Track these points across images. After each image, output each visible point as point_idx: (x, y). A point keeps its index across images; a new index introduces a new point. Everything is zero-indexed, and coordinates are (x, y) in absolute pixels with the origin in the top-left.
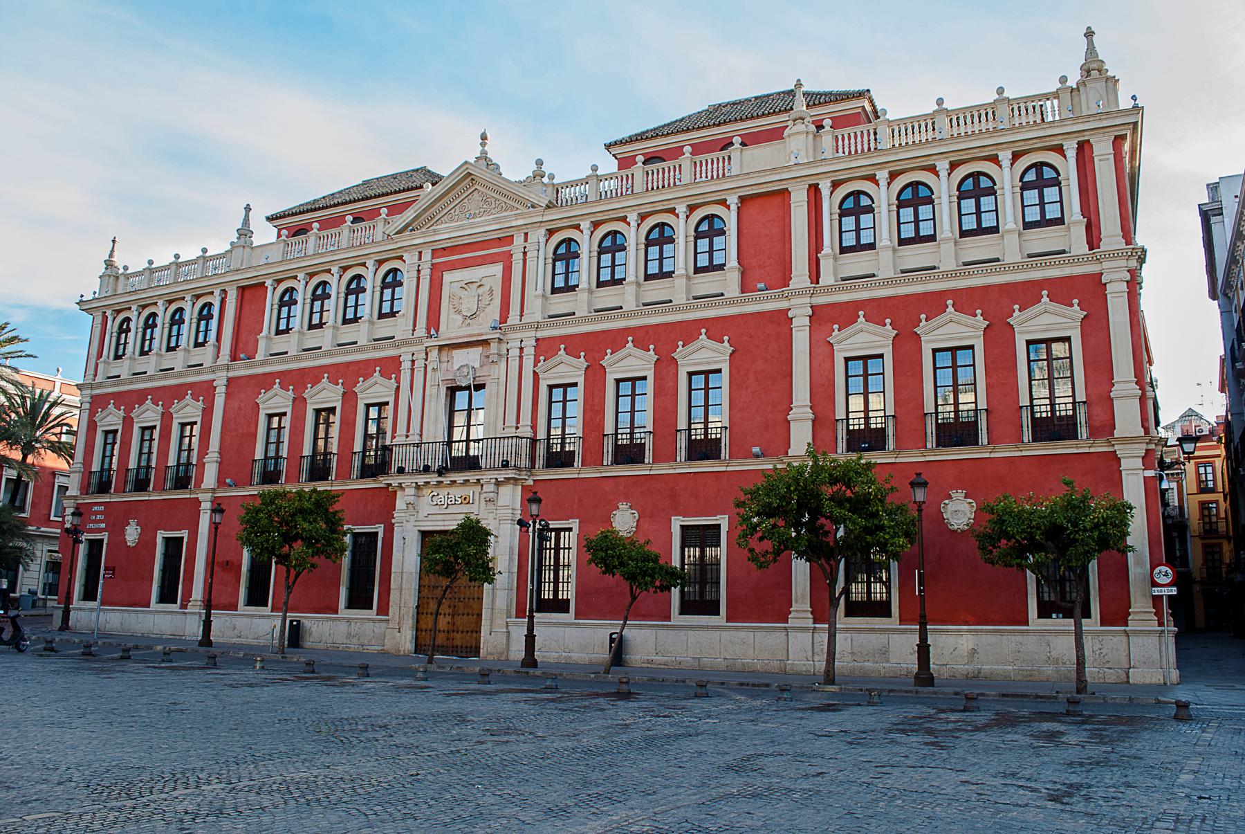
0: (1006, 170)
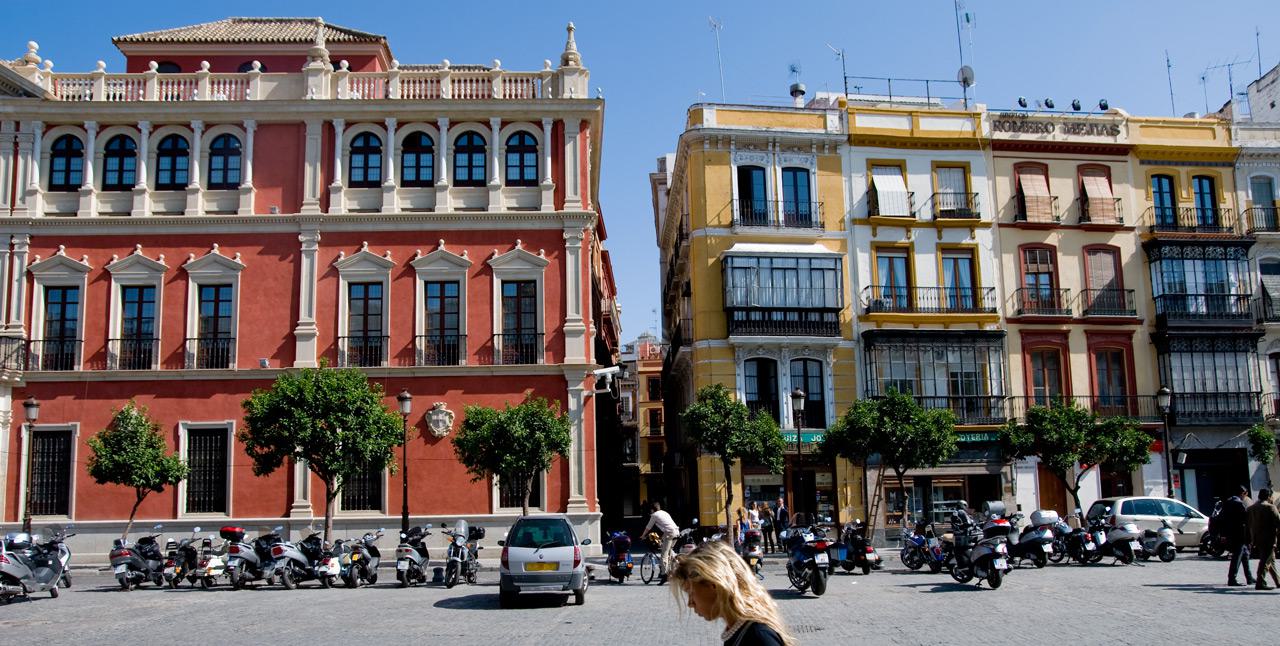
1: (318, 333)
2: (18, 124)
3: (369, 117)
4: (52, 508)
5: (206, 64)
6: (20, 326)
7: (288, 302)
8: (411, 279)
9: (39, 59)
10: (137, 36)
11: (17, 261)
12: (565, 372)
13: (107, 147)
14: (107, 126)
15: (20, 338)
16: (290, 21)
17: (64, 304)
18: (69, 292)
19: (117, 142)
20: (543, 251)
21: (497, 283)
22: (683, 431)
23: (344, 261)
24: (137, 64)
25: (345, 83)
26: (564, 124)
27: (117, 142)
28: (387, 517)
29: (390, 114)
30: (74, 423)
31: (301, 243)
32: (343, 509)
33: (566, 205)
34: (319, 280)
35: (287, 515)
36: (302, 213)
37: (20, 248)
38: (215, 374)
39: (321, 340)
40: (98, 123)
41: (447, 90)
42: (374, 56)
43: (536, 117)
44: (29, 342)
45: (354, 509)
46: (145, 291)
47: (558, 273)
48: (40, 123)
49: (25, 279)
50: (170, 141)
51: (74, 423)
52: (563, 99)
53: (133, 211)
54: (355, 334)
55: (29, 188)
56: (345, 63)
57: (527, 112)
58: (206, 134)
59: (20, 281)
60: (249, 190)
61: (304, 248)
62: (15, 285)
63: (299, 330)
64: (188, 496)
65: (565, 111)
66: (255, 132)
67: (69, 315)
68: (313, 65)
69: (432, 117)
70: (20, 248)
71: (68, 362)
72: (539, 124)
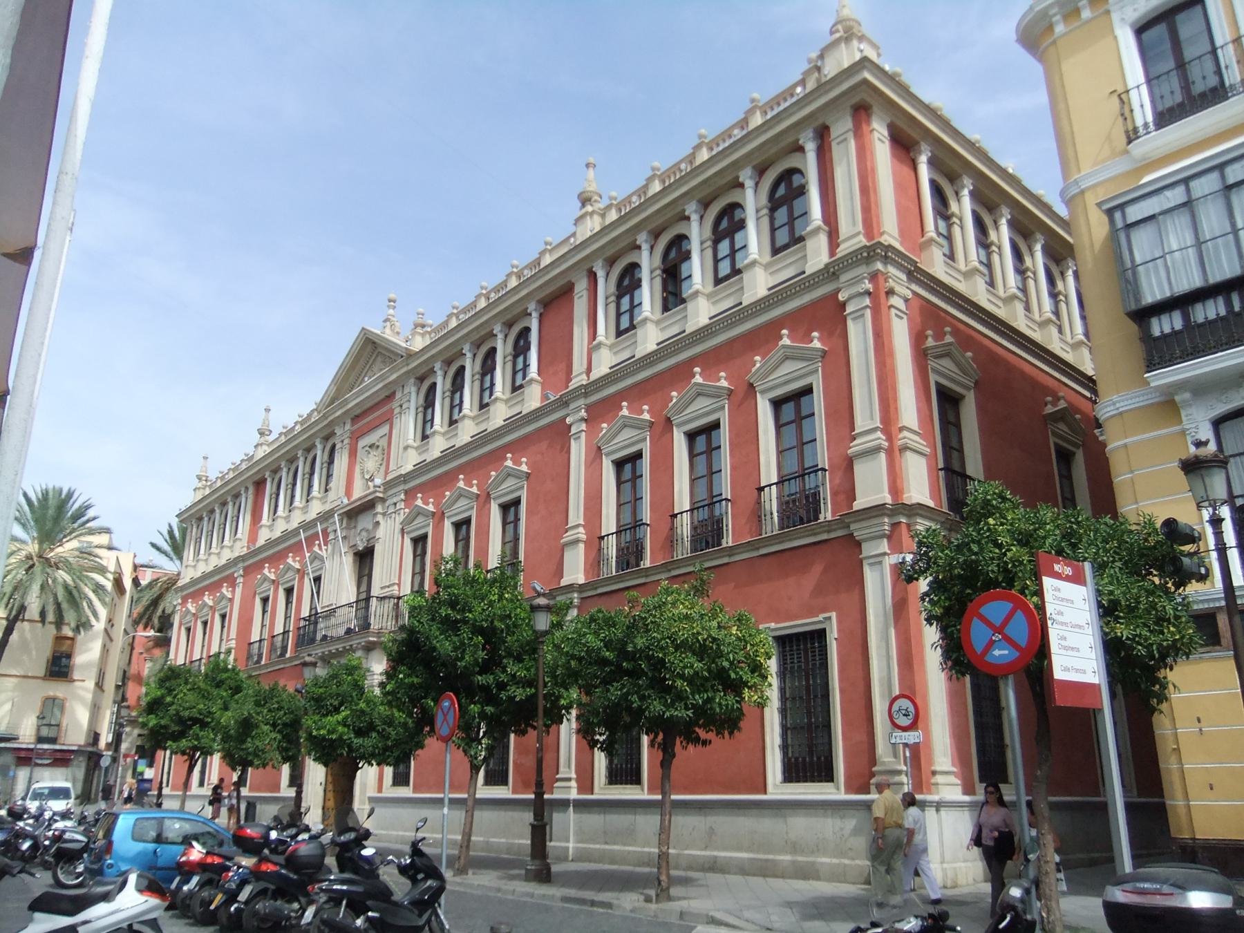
0: (749, 193)
6: (569, 779)
28: (645, 796)
29: (737, 165)
46: (998, 623)
66: (541, 315)
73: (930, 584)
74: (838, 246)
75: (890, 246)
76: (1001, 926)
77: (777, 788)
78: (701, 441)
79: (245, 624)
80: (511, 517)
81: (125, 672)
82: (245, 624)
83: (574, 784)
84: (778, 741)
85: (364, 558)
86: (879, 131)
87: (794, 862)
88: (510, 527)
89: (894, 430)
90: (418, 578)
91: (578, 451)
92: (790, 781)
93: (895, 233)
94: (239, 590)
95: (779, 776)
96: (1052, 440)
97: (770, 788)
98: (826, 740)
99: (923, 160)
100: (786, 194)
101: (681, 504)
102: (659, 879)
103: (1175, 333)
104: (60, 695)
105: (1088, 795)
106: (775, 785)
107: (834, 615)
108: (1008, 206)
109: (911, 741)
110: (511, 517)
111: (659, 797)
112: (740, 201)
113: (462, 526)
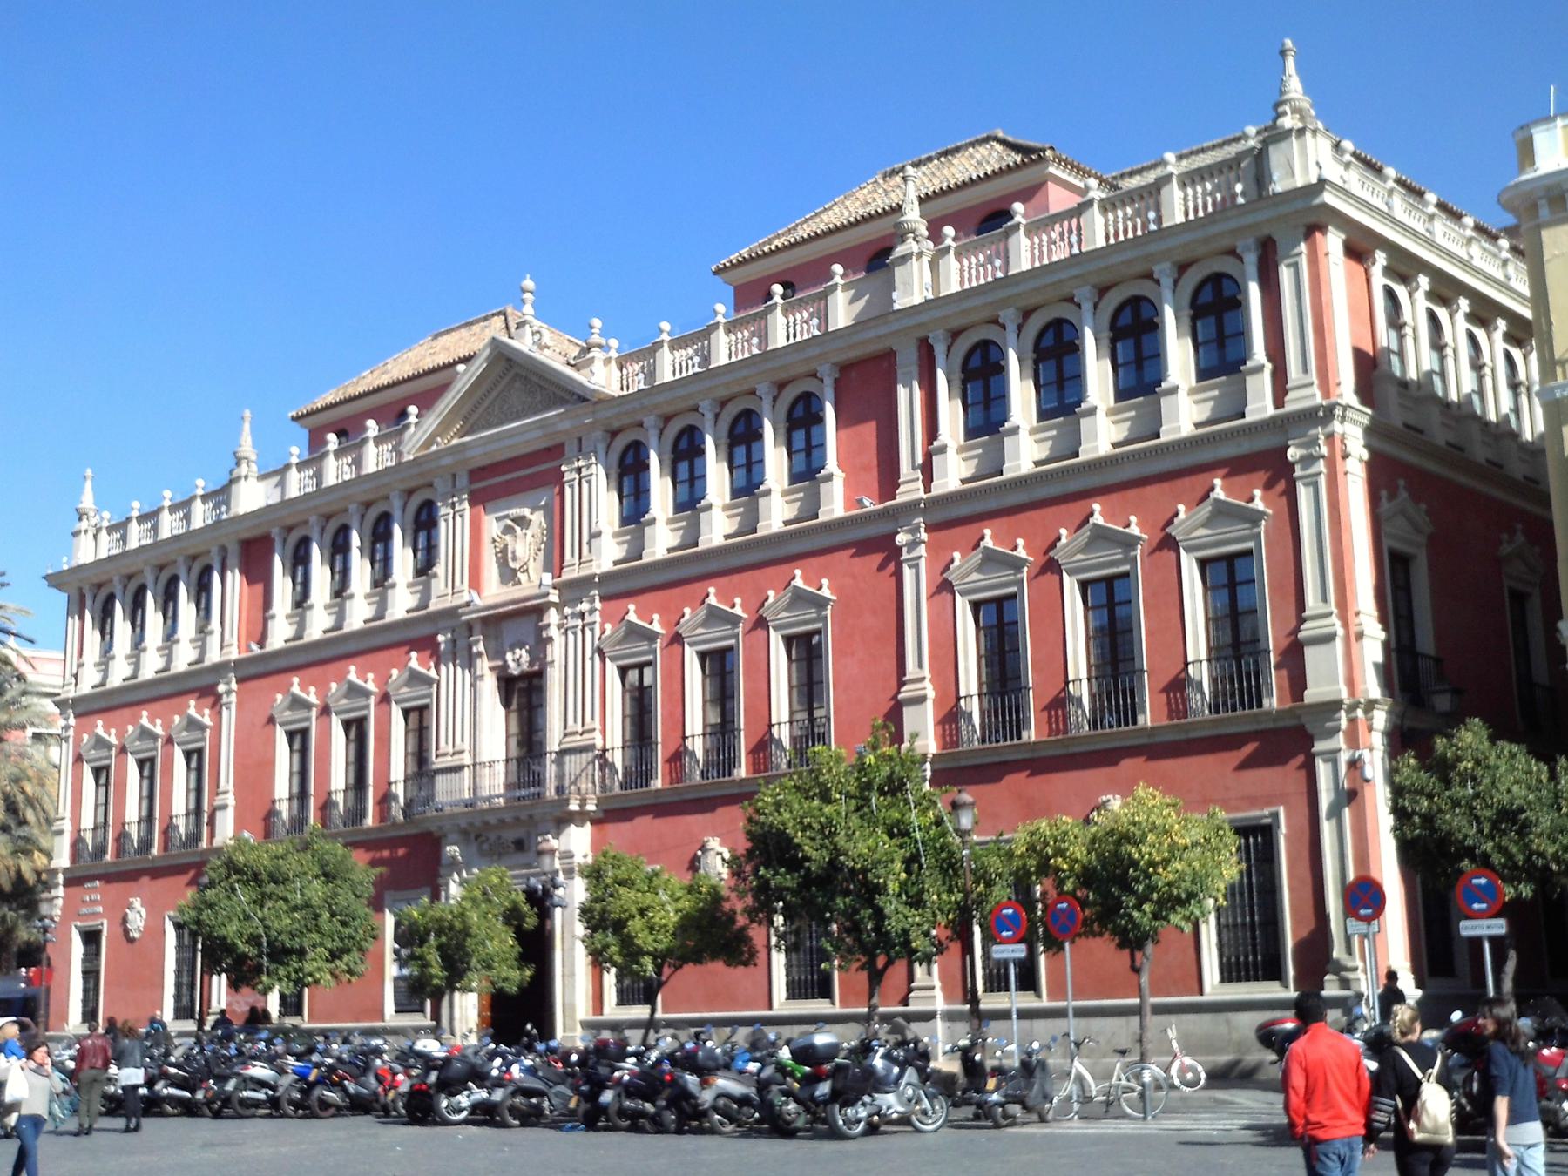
1: (931, 693)
2: (454, 476)
3: (975, 317)
4: (1256, 971)
5: (838, 269)
6: (923, 679)
7: (892, 650)
8: (1057, 578)
9: (603, 342)
10: (745, 252)
11: (588, 633)
12: (1304, 720)
13: (1194, 303)
14: (1035, 309)
15: (592, 747)
16: (957, 150)
17: (1232, 585)
18: (1238, 563)
19: (1208, 288)
20: (1133, 519)
21: (1189, 565)
22: (406, 908)
23: (1183, 522)
24: (348, 431)
25: (951, 263)
26: (1274, 242)
27: (1208, 288)
28: (837, 1009)
29: (1004, 303)
30: (1273, 809)
31: (1293, 464)
32: (1223, 980)
33: (1291, 396)
34: (930, 597)
35: (905, 1002)
36: (900, 499)
37: (909, 552)
38: (1114, 732)
39: (938, 702)
40: (1094, 286)
41: (1178, 207)
42: (1045, 183)
43: (1226, 243)
44: (605, 751)
45: (1248, 980)
46: (1116, 583)
47: (1288, 529)
48: (1012, 310)
49: (597, 657)
50: (1051, 331)
51: (1273, 809)
52: (1275, 195)
53: (1163, 429)
54: (1223, 654)
55: (594, 529)
56: (949, 231)
57: (1206, 240)
58: (779, 401)
59: (592, 659)
60: (1260, 369)
61: (1298, 472)
62: (588, 663)
63: (1308, 630)
64: (1221, 956)
65: (1268, 221)
66: (836, 381)
67: (1243, 605)
68: (900, 251)
69: (1065, 291)
70: (909, 552)
71: (1129, 713)
72: (1232, 252)
73: (247, 841)
74: (1286, 393)
75: (613, 765)
76: (1475, 881)
77: (1213, 985)
78: (414, 717)
79: (255, 772)
80: (102, 781)
81: (77, 1134)
82: (255, 772)
83: (938, 993)
84: (783, 980)
85: (523, 693)
86: (1333, 242)
87: (1142, 671)
88: (102, 790)
89: (1351, 614)
90: (101, 810)
91: (916, 583)
92: (1230, 980)
93: (1300, 89)
94: (229, 717)
95: (784, 994)
96: (1507, 583)
97: (387, 1017)
98: (1386, 528)
99: (1377, 271)
100: (1216, 316)
101: (967, 687)
102: (815, 1096)
103: (512, 649)
104: (505, 589)
105: (535, 413)
106: (1213, 987)
107: (1282, 810)
108: (1383, 250)
109: (1400, 985)
110: (102, 781)
111: (1137, 1001)
112: (698, 425)
113: (719, 664)
